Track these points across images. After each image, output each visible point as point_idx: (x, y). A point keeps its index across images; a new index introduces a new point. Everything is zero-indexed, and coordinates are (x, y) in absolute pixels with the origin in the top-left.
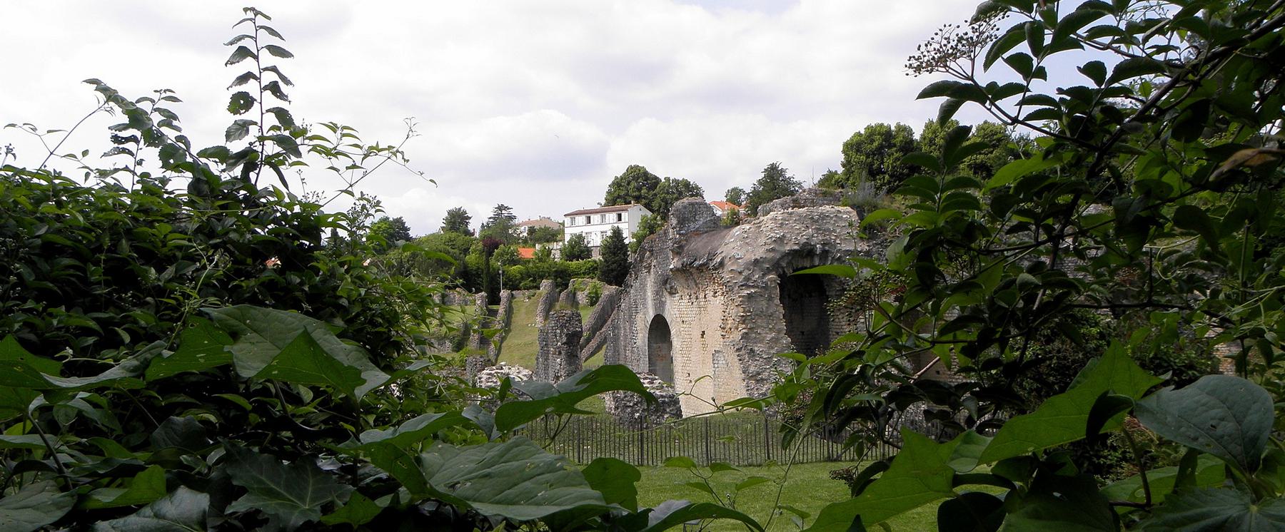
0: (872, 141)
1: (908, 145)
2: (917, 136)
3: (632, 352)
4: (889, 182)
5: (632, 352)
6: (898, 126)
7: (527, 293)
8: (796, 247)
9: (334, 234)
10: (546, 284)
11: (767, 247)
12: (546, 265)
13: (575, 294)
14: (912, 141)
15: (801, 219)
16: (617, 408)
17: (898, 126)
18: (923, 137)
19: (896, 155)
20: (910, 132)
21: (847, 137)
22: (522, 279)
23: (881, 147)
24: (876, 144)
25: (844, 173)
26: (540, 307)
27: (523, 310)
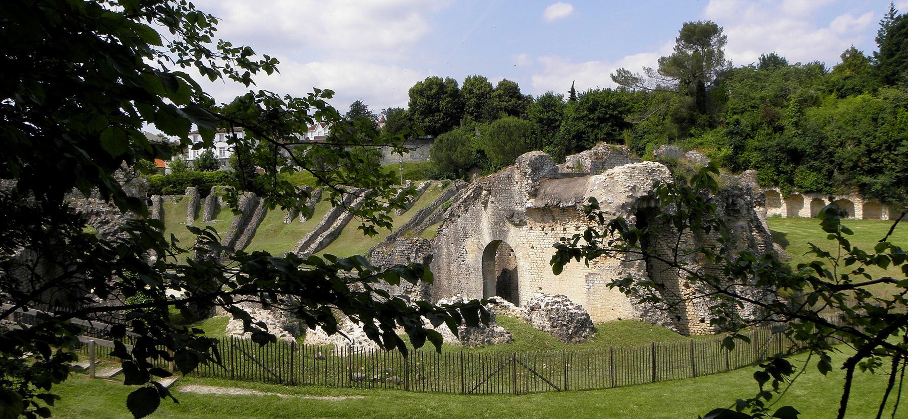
0: (431, 89)
1: (455, 93)
2: (460, 87)
3: (459, 268)
4: (443, 118)
5: (459, 268)
6: (448, 79)
7: (174, 197)
8: (646, 194)
9: (381, 208)
10: (190, 192)
11: (627, 194)
12: (185, 175)
13: (216, 198)
14: (457, 90)
15: (642, 172)
16: (553, 327)
17: (448, 79)
18: (465, 88)
19: (447, 99)
20: (456, 84)
21: (412, 84)
22: (163, 185)
23: (438, 93)
24: (434, 91)
25: (410, 110)
26: (190, 210)
27: (173, 212)
